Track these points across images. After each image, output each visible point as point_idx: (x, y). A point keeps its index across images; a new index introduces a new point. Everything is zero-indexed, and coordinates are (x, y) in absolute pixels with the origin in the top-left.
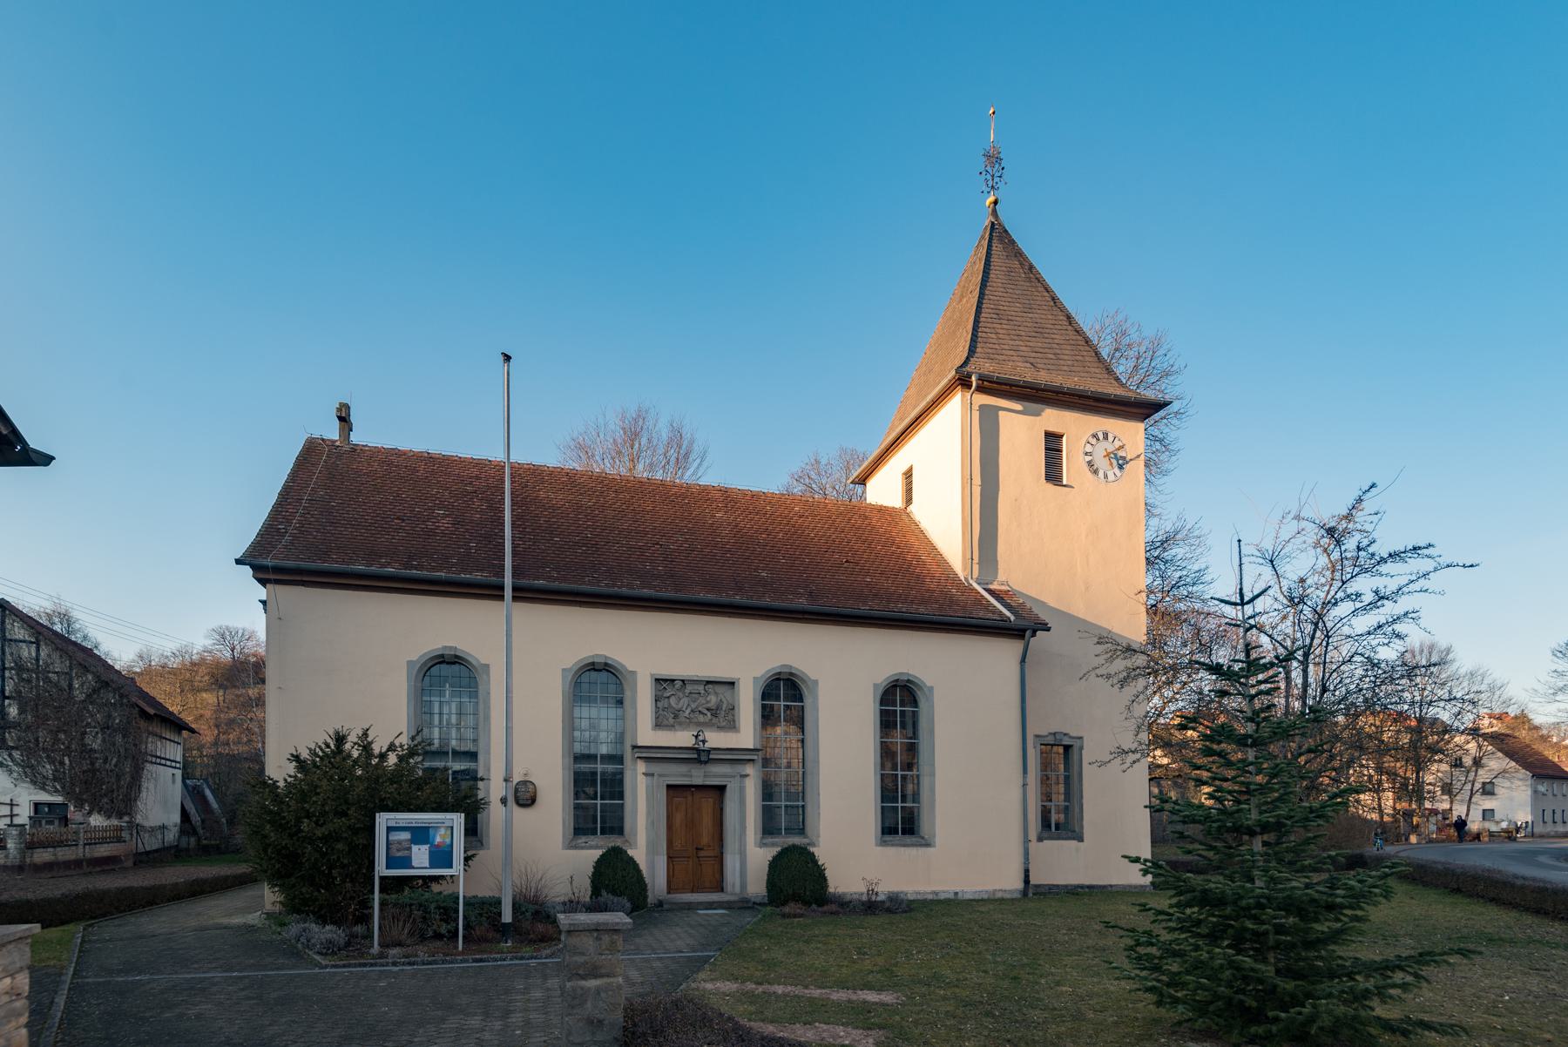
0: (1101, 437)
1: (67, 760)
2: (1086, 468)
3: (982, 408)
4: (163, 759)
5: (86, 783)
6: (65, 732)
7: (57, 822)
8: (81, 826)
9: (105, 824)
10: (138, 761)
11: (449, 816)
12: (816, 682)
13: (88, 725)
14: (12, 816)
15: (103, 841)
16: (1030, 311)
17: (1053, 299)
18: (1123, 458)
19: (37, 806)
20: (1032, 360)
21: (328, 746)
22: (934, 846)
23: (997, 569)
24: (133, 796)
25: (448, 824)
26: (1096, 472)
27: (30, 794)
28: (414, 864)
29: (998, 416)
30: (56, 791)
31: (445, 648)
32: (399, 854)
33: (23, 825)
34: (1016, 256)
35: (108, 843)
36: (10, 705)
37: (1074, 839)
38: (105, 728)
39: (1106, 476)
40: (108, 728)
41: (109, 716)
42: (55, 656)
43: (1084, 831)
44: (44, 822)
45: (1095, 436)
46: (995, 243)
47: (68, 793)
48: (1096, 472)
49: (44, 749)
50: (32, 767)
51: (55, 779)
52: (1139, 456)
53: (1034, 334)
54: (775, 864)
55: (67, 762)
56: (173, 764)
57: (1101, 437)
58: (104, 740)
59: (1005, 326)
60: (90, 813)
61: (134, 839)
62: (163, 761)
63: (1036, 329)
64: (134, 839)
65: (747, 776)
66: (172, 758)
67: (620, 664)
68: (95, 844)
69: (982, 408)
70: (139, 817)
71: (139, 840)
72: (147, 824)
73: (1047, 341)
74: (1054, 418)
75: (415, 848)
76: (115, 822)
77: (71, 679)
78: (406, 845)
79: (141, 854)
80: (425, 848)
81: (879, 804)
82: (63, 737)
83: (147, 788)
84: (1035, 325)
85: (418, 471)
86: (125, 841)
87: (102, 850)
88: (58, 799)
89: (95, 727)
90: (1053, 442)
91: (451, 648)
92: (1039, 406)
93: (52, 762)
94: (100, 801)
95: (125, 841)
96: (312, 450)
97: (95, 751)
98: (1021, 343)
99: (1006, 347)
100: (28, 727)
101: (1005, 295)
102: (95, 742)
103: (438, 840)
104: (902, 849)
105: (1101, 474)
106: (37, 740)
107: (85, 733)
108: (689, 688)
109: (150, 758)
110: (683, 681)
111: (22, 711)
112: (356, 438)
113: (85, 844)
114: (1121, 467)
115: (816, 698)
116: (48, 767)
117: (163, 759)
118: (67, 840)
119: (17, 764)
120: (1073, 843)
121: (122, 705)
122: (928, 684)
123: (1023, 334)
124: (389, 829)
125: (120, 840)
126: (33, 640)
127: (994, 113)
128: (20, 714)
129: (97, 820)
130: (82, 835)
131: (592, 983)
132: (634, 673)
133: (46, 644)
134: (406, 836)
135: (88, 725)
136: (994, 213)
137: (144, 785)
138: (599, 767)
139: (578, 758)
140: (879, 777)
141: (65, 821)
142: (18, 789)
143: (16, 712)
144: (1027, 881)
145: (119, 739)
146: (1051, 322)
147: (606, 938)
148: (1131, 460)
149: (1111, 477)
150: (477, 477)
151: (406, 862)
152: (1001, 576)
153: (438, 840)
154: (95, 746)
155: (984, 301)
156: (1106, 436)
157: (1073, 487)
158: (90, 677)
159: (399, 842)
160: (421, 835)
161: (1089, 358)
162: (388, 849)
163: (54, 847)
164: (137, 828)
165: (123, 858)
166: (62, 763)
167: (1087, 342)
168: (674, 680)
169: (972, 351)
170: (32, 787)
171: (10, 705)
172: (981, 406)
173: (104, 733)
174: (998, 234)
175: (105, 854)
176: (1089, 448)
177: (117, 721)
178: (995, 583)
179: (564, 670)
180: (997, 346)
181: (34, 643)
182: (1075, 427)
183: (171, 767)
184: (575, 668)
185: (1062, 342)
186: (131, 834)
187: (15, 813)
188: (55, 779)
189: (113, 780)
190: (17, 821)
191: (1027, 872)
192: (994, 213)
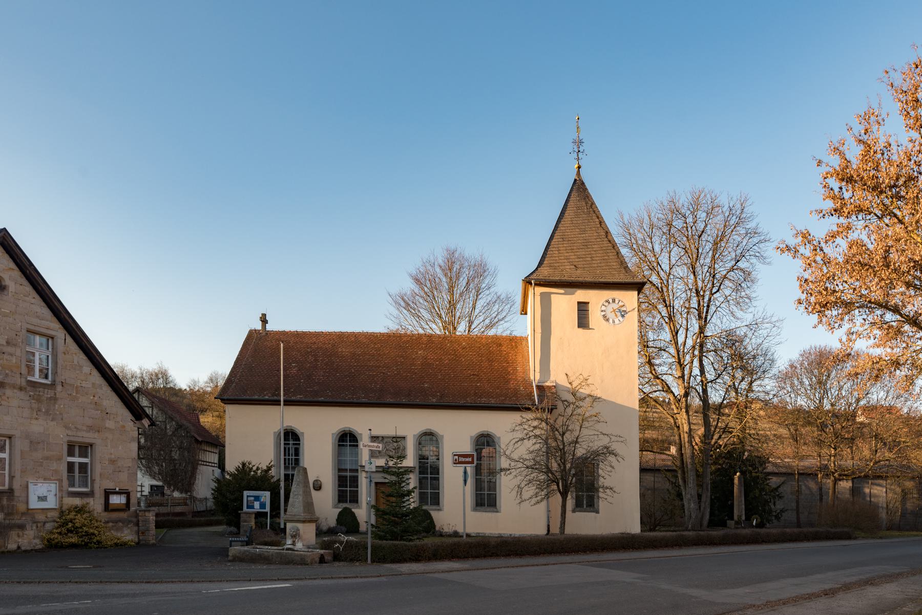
0: (611, 301)
1: (164, 464)
2: (602, 318)
3: (542, 294)
4: (213, 463)
5: (172, 476)
6: (163, 450)
7: (160, 495)
8: (170, 497)
9: (180, 496)
10: (194, 465)
11: (265, 492)
12: (443, 436)
13: (173, 447)
14: (142, 491)
15: (179, 504)
16: (584, 232)
17: (600, 223)
18: (625, 311)
19: (152, 486)
20: (575, 263)
21: (239, 467)
22: (500, 512)
23: (550, 374)
24: (192, 482)
25: (265, 495)
26: (608, 320)
27: (149, 481)
28: (255, 507)
29: (551, 297)
30: (160, 480)
31: (427, 429)
32: (251, 504)
33: (146, 496)
34: (585, 199)
35: (181, 505)
36: (141, 438)
37: (594, 512)
38: (180, 448)
39: (614, 322)
40: (181, 448)
41: (182, 442)
42: (160, 413)
43: (600, 508)
44: (154, 495)
45: (607, 301)
46: (574, 194)
47: (164, 481)
48: (608, 320)
49: (155, 459)
50: (150, 468)
51: (159, 474)
52: (634, 309)
53: (582, 247)
54: (340, 514)
55: (164, 465)
56: (213, 465)
57: (611, 301)
58: (179, 454)
59: (565, 245)
60: (173, 491)
61: (192, 504)
62: (207, 463)
63: (583, 244)
64: (192, 504)
65: (410, 478)
66: (212, 462)
67: (355, 430)
68: (175, 506)
69: (542, 294)
70: (194, 493)
71: (195, 506)
72: (198, 497)
73: (589, 250)
74: (582, 295)
75: (255, 503)
76: (184, 495)
77: (166, 425)
78: (253, 501)
79: (195, 512)
80: (258, 503)
81: (337, 488)
82: (162, 453)
83: (199, 478)
84: (585, 241)
85: (290, 343)
86: (188, 505)
87: (178, 509)
88: (160, 483)
89: (176, 448)
90: (583, 308)
91: (289, 426)
92: (574, 289)
93: (158, 465)
94: (178, 485)
95: (188, 505)
96: (252, 334)
97: (176, 460)
98: (572, 254)
99: (563, 258)
100: (148, 448)
101: (571, 225)
102: (176, 455)
103: (262, 500)
104: (484, 513)
105: (611, 321)
106: (152, 454)
107: (171, 451)
108: (386, 440)
109: (200, 462)
110: (383, 437)
111: (146, 441)
112: (269, 327)
113: (171, 506)
114: (623, 316)
115: (442, 443)
116: (156, 467)
117: (213, 463)
118: (164, 503)
119: (144, 466)
120: (593, 514)
121: (187, 437)
122: (498, 436)
123: (575, 248)
124: (248, 496)
125: (186, 504)
126: (150, 406)
127: (578, 119)
128: (145, 442)
129: (176, 494)
130: (169, 501)
131: (245, 524)
132: (361, 434)
133: (156, 408)
134: (252, 498)
135: (173, 447)
136: (578, 173)
137: (197, 477)
138: (348, 474)
139: (340, 470)
140: (475, 479)
141: (163, 494)
142: (144, 478)
143: (144, 441)
144: (549, 531)
145: (186, 454)
146: (595, 237)
147: (248, 515)
148: (629, 312)
149: (617, 321)
150: (315, 343)
151: (253, 507)
152: (552, 378)
153: (262, 500)
154: (176, 457)
155: (557, 232)
156: (614, 301)
157: (593, 329)
158: (174, 423)
159: (251, 501)
160: (257, 498)
161: (612, 255)
162: (247, 503)
163: (159, 506)
164: (192, 498)
165: (187, 513)
166: (162, 466)
167: (614, 247)
168: (378, 437)
169: (540, 264)
170: (150, 477)
171: (141, 438)
172: (541, 293)
173: (179, 451)
174: (579, 187)
175: (180, 511)
176: (604, 308)
177: (185, 445)
178: (549, 382)
179: (332, 434)
180: (557, 258)
181: (150, 407)
182: (596, 299)
183: (212, 466)
184: (476, 436)
185: (598, 249)
186: (191, 502)
187: (143, 490)
188: (159, 474)
189: (183, 474)
190: (144, 494)
191: (548, 526)
192: (578, 173)
